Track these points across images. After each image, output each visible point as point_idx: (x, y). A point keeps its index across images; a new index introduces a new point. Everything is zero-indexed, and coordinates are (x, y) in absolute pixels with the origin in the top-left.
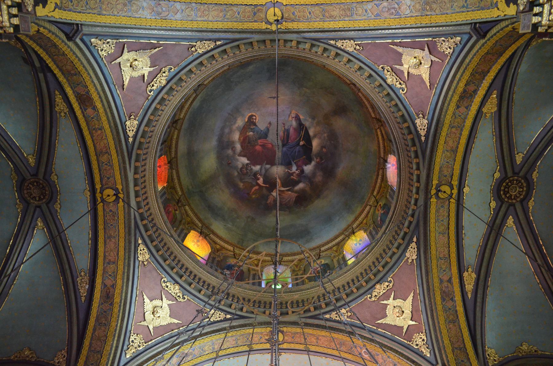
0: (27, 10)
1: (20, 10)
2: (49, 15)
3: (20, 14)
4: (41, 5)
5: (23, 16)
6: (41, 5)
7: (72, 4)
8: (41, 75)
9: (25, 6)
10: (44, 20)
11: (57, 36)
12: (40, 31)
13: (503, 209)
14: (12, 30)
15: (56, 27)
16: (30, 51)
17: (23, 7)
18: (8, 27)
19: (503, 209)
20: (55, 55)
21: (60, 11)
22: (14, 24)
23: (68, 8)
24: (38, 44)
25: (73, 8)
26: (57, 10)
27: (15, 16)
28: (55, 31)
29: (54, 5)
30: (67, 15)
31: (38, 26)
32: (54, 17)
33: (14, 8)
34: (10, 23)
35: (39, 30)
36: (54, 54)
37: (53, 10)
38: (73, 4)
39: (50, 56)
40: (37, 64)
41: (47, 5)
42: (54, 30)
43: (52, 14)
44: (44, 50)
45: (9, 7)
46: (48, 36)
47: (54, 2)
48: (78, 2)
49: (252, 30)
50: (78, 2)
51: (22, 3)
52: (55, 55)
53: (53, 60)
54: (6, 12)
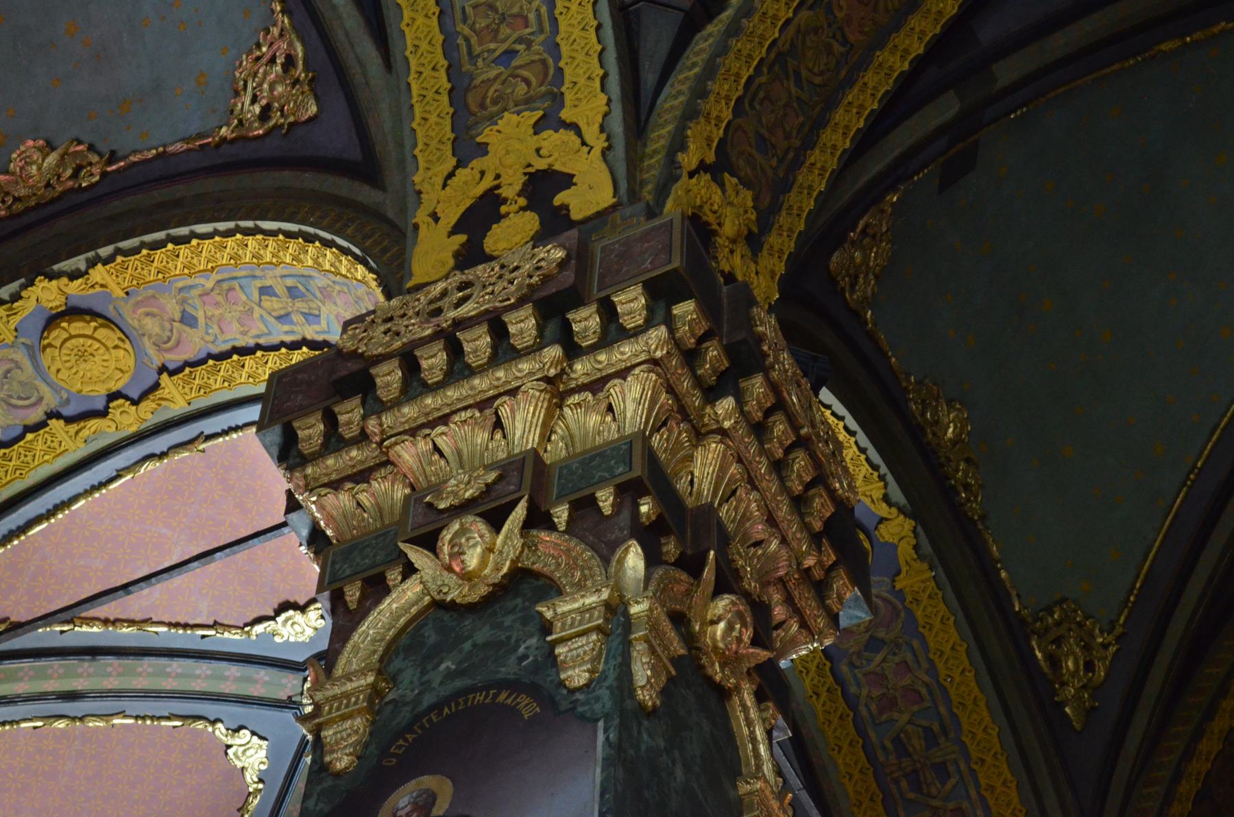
0: (562, 264)
1: (575, 298)
2: (599, 143)
3: (596, 293)
4: (559, 200)
5: (602, 277)
6: (559, 200)
7: (520, 47)
8: (1006, 72)
9: (546, 279)
10: (634, 161)
11: (710, 71)
12: (711, 158)
13: (286, 685)
14: (685, 309)
15: (667, 90)
16: (875, 166)
17: (552, 289)
18: (671, 331)
19: (286, 685)
20: (845, 41)
21: (569, 98)
22: (650, 309)
23: (544, 62)
24: (809, 143)
25: (541, 38)
26: (566, 114)
27: (608, 312)
28: (684, 88)
29: (545, 134)
30: (580, 57)
31: (677, 179)
32: (606, 115)
33: (576, 328)
34: (649, 324)
35: (702, 167)
36: (838, 48)
37: (571, 136)
38: (520, 40)
39: (863, 64)
40: (946, 109)
41: (557, 167)
42: (680, 93)
43: (592, 133)
44: (831, 104)
45: (573, 351)
46: (727, 115)
47: (534, 142)
48: (503, 18)
49: (408, 143)
50: (503, 18)
51: (537, 296)
52: (845, 41)
53: (880, 39)
54: (602, 357)
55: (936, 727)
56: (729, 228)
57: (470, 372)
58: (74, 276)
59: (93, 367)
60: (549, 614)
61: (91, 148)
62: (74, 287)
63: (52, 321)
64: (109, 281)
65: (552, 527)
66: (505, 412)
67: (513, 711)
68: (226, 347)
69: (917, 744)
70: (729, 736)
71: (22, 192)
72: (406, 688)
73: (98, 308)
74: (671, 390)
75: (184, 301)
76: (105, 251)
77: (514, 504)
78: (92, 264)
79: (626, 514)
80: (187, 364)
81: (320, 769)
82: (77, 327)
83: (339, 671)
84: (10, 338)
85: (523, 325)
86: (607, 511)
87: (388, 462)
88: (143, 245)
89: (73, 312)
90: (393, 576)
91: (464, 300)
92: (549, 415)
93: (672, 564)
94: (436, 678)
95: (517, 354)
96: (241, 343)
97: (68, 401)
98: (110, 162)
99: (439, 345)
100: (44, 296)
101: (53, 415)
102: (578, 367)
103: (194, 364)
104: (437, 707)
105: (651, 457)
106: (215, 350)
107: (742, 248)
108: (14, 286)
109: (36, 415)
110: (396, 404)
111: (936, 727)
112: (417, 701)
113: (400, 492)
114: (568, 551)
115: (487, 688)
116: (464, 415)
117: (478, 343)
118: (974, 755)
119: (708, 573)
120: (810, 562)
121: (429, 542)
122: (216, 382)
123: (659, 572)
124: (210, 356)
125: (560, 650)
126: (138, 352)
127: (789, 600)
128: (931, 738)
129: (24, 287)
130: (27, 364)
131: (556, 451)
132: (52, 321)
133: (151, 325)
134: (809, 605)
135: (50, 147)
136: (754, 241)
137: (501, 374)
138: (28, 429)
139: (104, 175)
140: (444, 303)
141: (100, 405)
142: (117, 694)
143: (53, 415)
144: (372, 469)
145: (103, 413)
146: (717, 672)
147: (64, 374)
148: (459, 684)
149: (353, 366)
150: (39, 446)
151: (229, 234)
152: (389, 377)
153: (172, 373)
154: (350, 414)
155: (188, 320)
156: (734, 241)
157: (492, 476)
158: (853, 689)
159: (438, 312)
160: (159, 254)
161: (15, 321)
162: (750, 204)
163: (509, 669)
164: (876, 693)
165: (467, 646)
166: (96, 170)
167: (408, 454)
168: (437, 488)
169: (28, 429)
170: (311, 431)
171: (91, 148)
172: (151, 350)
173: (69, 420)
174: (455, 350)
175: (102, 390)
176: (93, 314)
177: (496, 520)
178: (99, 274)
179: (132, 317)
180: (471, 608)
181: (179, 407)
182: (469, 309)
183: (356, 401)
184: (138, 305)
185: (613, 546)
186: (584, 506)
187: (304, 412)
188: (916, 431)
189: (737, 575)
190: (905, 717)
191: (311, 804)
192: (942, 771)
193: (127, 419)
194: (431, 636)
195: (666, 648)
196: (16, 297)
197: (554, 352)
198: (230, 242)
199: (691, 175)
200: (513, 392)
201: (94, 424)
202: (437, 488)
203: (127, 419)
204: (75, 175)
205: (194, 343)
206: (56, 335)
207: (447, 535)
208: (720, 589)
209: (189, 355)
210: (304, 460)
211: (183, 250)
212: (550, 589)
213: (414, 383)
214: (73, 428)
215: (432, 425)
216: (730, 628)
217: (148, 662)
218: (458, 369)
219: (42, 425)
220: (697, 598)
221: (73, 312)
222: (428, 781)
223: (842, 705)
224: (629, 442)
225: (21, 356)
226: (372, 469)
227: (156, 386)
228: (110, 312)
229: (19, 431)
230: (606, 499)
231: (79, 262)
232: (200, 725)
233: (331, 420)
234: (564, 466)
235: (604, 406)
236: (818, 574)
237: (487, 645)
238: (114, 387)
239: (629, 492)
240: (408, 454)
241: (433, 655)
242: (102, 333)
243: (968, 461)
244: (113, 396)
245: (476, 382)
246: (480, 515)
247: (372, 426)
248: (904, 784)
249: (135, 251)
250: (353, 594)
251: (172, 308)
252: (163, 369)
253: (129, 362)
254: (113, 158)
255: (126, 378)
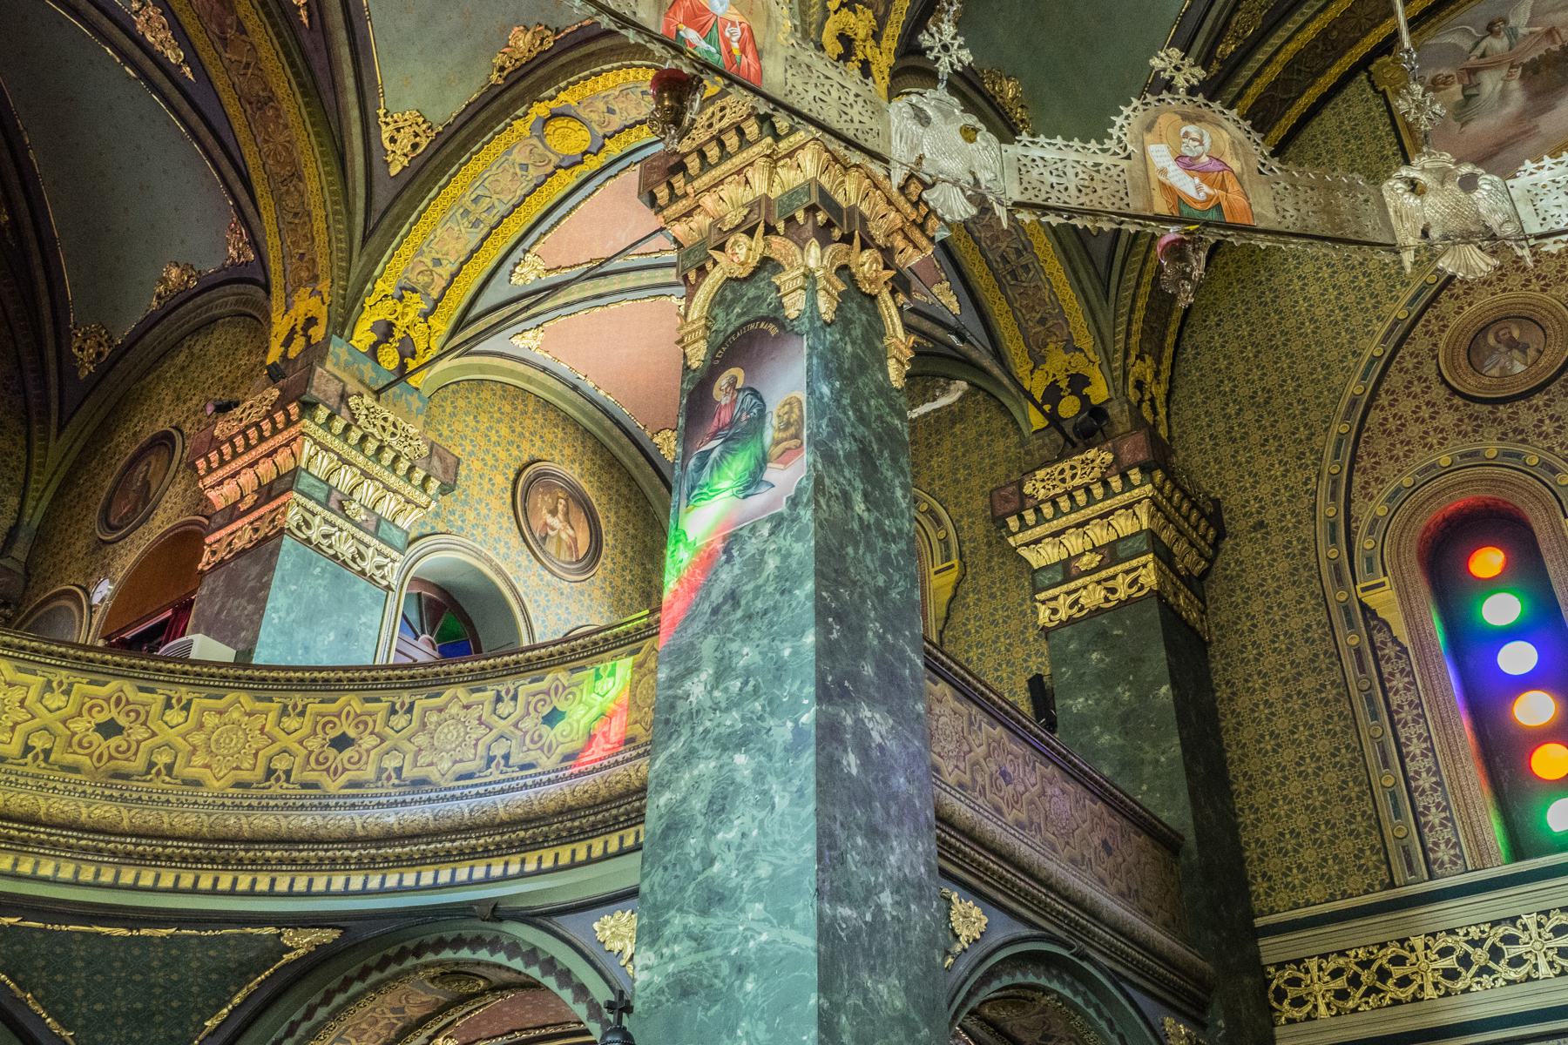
45: (777, 138)
54: (792, 139)
55: (1021, 247)
56: (862, 34)
57: (730, 156)
58: (551, 99)
59: (572, 142)
60: (778, 283)
61: (546, 27)
62: (553, 105)
63: (546, 122)
64: (568, 98)
65: (778, 234)
66: (749, 175)
67: (767, 332)
68: (632, 121)
69: (1013, 257)
70: (879, 318)
71: (518, 56)
72: (719, 325)
73: (566, 112)
74: (827, 150)
75: (607, 103)
76: (562, 84)
77: (758, 224)
78: (558, 91)
79: (810, 222)
80: (616, 132)
81: (687, 368)
82: (559, 123)
83: (689, 319)
84: (528, 134)
85: (752, 129)
86: (802, 222)
87: (699, 206)
88: (580, 79)
89: (555, 115)
90: (709, 265)
91: (723, 117)
92: (771, 173)
93: (839, 241)
94: (733, 317)
95: (751, 144)
96: (639, 118)
97: (563, 160)
98: (557, 34)
99: (714, 143)
100: (539, 111)
101: (558, 167)
102: (781, 145)
103: (619, 132)
104: (734, 332)
105: (821, 190)
106: (627, 123)
107: (871, 42)
108: (523, 109)
109: (550, 169)
110: (698, 176)
111: (1021, 247)
112: (725, 330)
113: (709, 221)
114: (785, 246)
115: (755, 321)
116: (730, 179)
117: (732, 141)
118: (1041, 257)
119: (857, 242)
120: (913, 216)
121: (721, 248)
122: (632, 139)
123: (830, 249)
124: (626, 127)
125: (785, 300)
126: (590, 129)
127: (906, 237)
128: (1019, 253)
129: (529, 108)
130: (540, 145)
131: (776, 192)
132: (546, 122)
133: (594, 116)
134: (916, 235)
135: (527, 29)
136: (876, 36)
137: (745, 155)
138: (548, 176)
139: (555, 41)
140: (714, 120)
141: (579, 159)
142: (621, 292)
143: (558, 167)
144: (694, 209)
145: (582, 162)
146: (867, 288)
147: (558, 147)
148: (743, 320)
149: (676, 159)
150: (555, 183)
151: (619, 68)
152: (693, 163)
153: (610, 138)
154: (679, 181)
155: (611, 111)
156: (864, 41)
157: (745, 212)
158: (977, 234)
159: (711, 125)
160: (588, 83)
161: (528, 125)
162: (871, 16)
163: (763, 310)
164: (989, 235)
165: (745, 299)
166: (551, 39)
167: (708, 201)
168: (722, 219)
169: (548, 176)
170: (662, 193)
171: (546, 27)
172: (597, 128)
173: (566, 168)
174: (722, 145)
175: (578, 151)
176: (563, 115)
177: (750, 233)
178: (562, 96)
179: (584, 114)
180: (745, 279)
181: (617, 153)
182: (725, 123)
183: (681, 175)
184: (585, 108)
185: (806, 241)
186: (791, 220)
187: (658, 183)
188: (990, 100)
189: (872, 239)
190: (1005, 245)
191: (685, 386)
192: (1026, 268)
193: (593, 163)
194: (729, 295)
195: (836, 289)
196: (526, 114)
197: (769, 140)
198: (621, 72)
199: (836, 12)
200: (751, 164)
201: (578, 169)
202: (722, 219)
203: (593, 163)
204: (541, 44)
205: (616, 122)
206: (549, 129)
207: (728, 245)
208: (864, 246)
209: (616, 127)
210: (662, 209)
211: (600, 79)
212: (778, 268)
213: (705, 166)
214: (569, 171)
215: (716, 185)
216: (871, 266)
217: (632, 274)
218: (725, 156)
219: (553, 173)
220: (853, 256)
221: (555, 115)
222: (734, 371)
223: (973, 244)
224: (809, 183)
225: (535, 141)
226: (694, 209)
227: (603, 145)
228: (572, 112)
229: (543, 178)
230: (800, 216)
231: (551, 91)
232: (664, 298)
233: (671, 186)
234: (779, 199)
235: (795, 165)
236: (920, 220)
237: (754, 298)
238: (583, 149)
239: (812, 210)
240: (708, 201)
241: (729, 307)
242: (572, 124)
243: (1022, 107)
244: (584, 153)
245: (734, 160)
246: (743, 232)
247: (689, 189)
248: (1009, 277)
249: (577, 82)
250: (692, 276)
251: (602, 107)
252: (605, 136)
253: (588, 136)
254: (557, 32)
255: (588, 144)
